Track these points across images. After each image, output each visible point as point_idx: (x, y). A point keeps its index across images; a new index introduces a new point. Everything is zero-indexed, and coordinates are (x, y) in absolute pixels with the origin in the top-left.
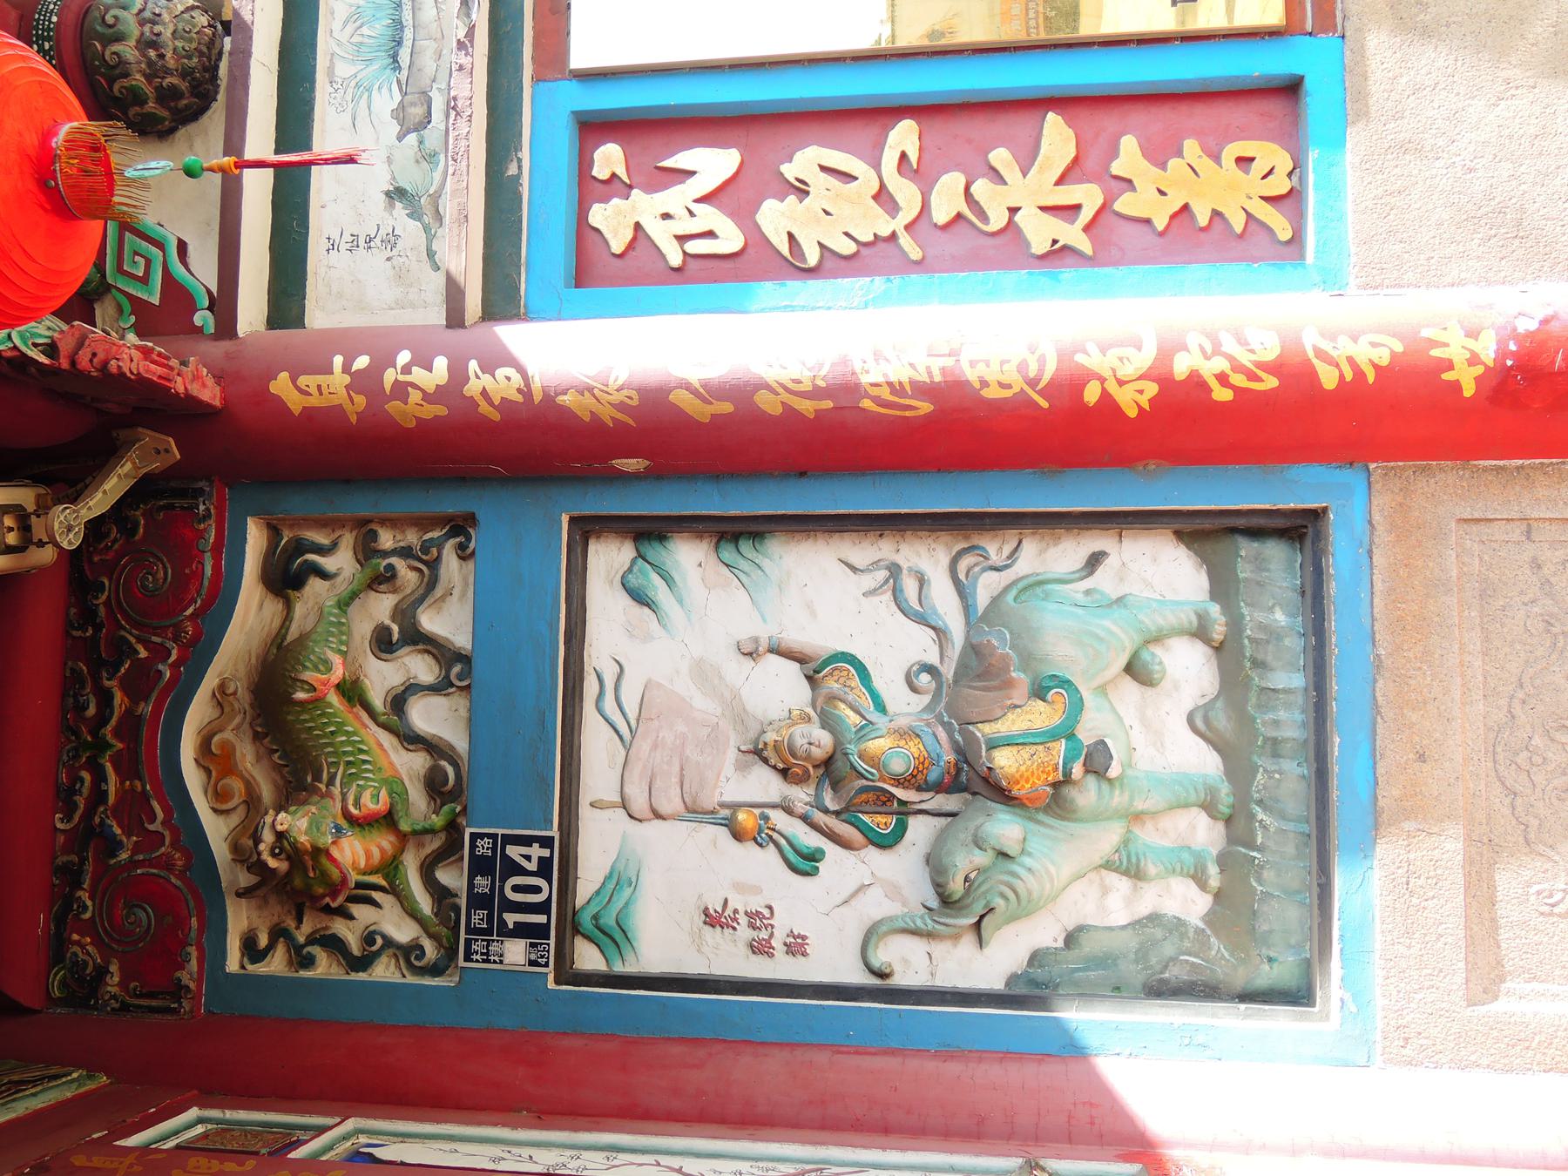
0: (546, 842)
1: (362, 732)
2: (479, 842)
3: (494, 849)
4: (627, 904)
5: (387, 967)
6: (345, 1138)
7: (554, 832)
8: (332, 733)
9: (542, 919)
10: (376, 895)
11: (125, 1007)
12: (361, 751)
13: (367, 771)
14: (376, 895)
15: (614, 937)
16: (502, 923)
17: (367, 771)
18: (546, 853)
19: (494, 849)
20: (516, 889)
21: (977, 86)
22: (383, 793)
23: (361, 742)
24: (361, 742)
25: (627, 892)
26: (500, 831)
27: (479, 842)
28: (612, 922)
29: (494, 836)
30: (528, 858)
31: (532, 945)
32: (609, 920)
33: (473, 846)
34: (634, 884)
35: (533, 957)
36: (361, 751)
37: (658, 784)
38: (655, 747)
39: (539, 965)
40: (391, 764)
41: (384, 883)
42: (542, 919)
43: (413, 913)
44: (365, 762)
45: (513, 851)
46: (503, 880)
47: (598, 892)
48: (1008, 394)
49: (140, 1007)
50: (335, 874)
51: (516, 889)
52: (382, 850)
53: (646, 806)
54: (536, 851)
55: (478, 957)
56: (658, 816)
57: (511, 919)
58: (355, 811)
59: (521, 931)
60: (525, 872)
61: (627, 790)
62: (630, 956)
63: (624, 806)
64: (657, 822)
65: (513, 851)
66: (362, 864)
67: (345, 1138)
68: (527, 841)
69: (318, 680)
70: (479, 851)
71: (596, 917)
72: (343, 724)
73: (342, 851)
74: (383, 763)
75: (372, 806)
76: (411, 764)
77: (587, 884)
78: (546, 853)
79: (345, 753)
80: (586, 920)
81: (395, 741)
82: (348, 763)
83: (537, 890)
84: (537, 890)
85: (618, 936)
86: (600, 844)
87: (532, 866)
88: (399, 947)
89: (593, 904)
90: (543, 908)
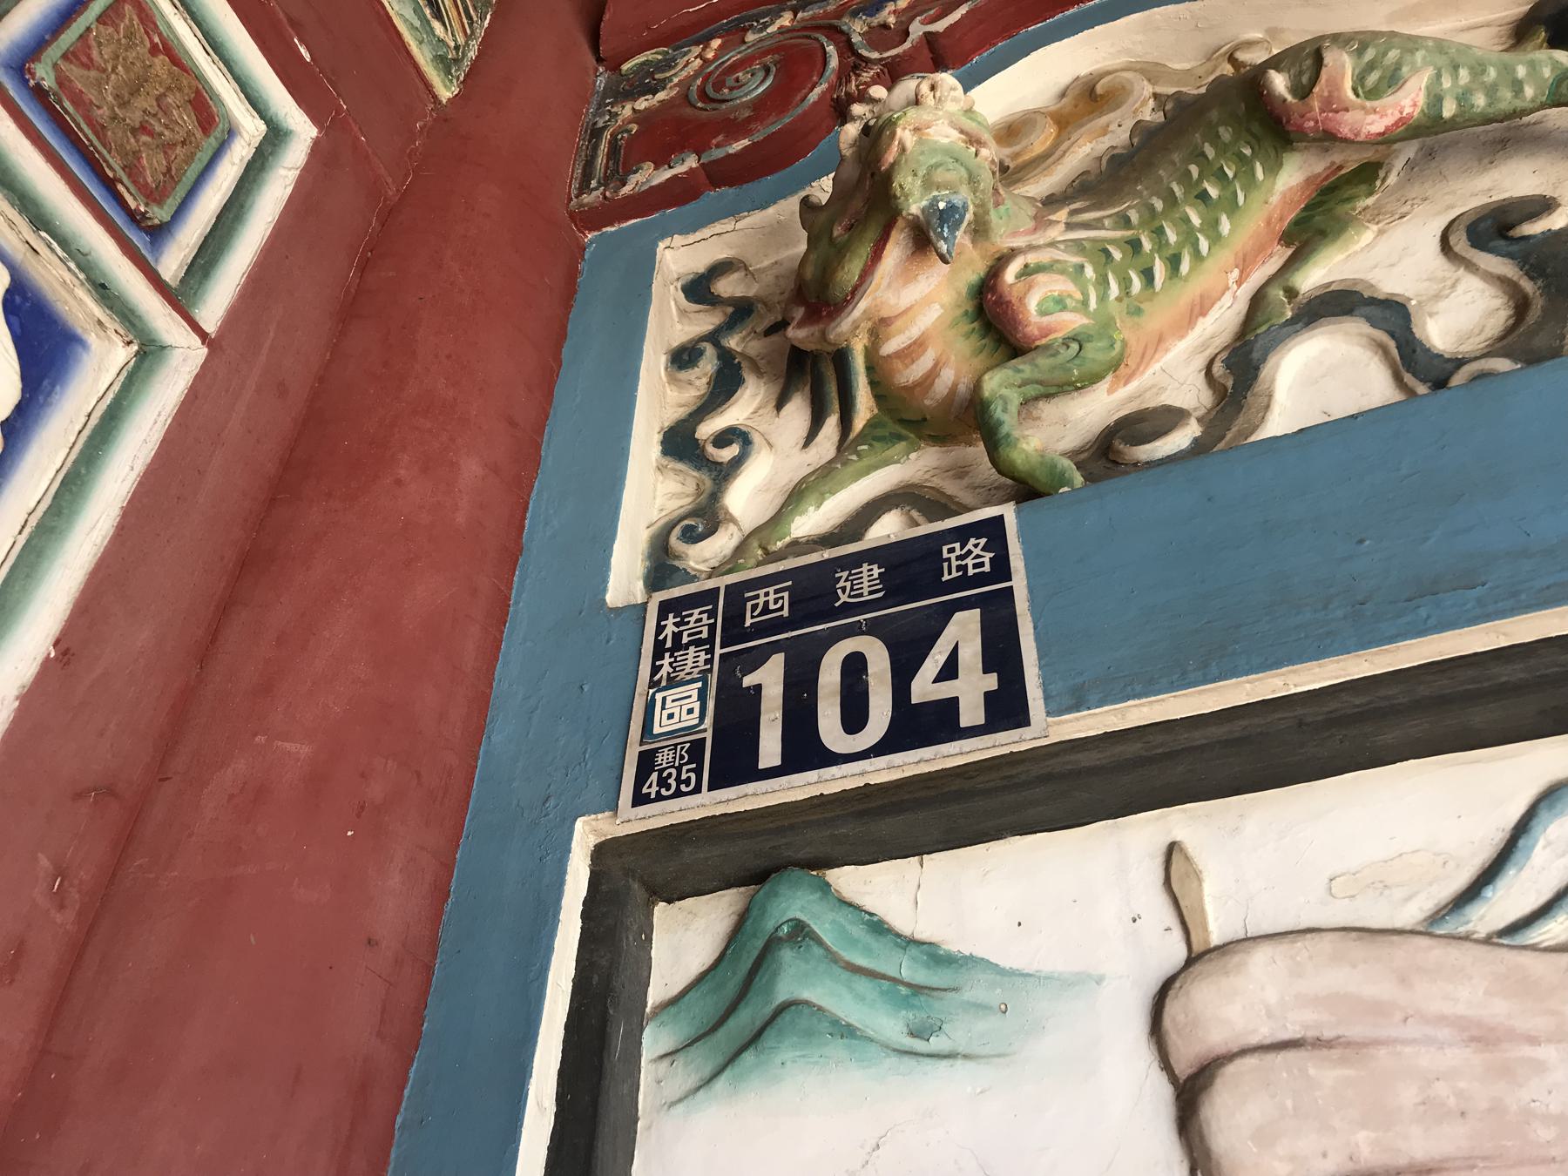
0: (1007, 708)
1: (1225, 256)
2: (976, 545)
3: (964, 582)
4: (847, 1032)
5: (675, 496)
6: (103, 290)
7: (1048, 727)
8: (1203, 196)
9: (770, 749)
10: (831, 424)
11: (596, 133)
12: (1174, 262)
13: (1125, 284)
14: (831, 424)
15: (743, 1016)
16: (756, 659)
17: (1125, 284)
18: (972, 713)
19: (964, 582)
20: (855, 667)
21: (524, 1131)
22: (1072, 321)
23: (1197, 256)
24: (1197, 256)
25: (889, 1025)
26: (1019, 583)
27: (976, 545)
28: (785, 989)
29: (1001, 568)
30: (949, 671)
31: (696, 749)
32: (795, 980)
33: (963, 534)
34: (923, 1044)
35: (663, 759)
36: (1174, 262)
37: (1324, 1074)
38: (1483, 1037)
39: (640, 779)
40: (1159, 342)
41: (859, 423)
42: (770, 749)
43: (797, 496)
44: (1148, 275)
45: (964, 632)
46: (873, 629)
47: (879, 927)
48: (778, 1060)
49: (595, 148)
50: (851, 270)
51: (855, 667)
52: (933, 374)
53: (1216, 1038)
54: (972, 691)
55: (670, 629)
56: (1190, 1094)
57: (770, 678)
58: (1010, 274)
59: (736, 715)
60: (903, 674)
61: (1261, 957)
62: (682, 1076)
63: (1191, 961)
64: (1160, 1093)
65: (964, 632)
66: (890, 347)
67: (103, 290)
68: (1001, 652)
69: (1335, 85)
70: (951, 552)
71: (800, 932)
72: (1232, 207)
73: (906, 275)
74: (1158, 316)
75: (1032, 303)
76: (1176, 375)
77: (896, 891)
78: (972, 713)
79: (1159, 232)
80: (793, 903)
81: (1225, 338)
82: (1135, 245)
83: (854, 718)
84: (854, 718)
85: (746, 1018)
86: (1048, 905)
87: (924, 687)
88: (715, 496)
89: (844, 917)
90: (805, 750)
